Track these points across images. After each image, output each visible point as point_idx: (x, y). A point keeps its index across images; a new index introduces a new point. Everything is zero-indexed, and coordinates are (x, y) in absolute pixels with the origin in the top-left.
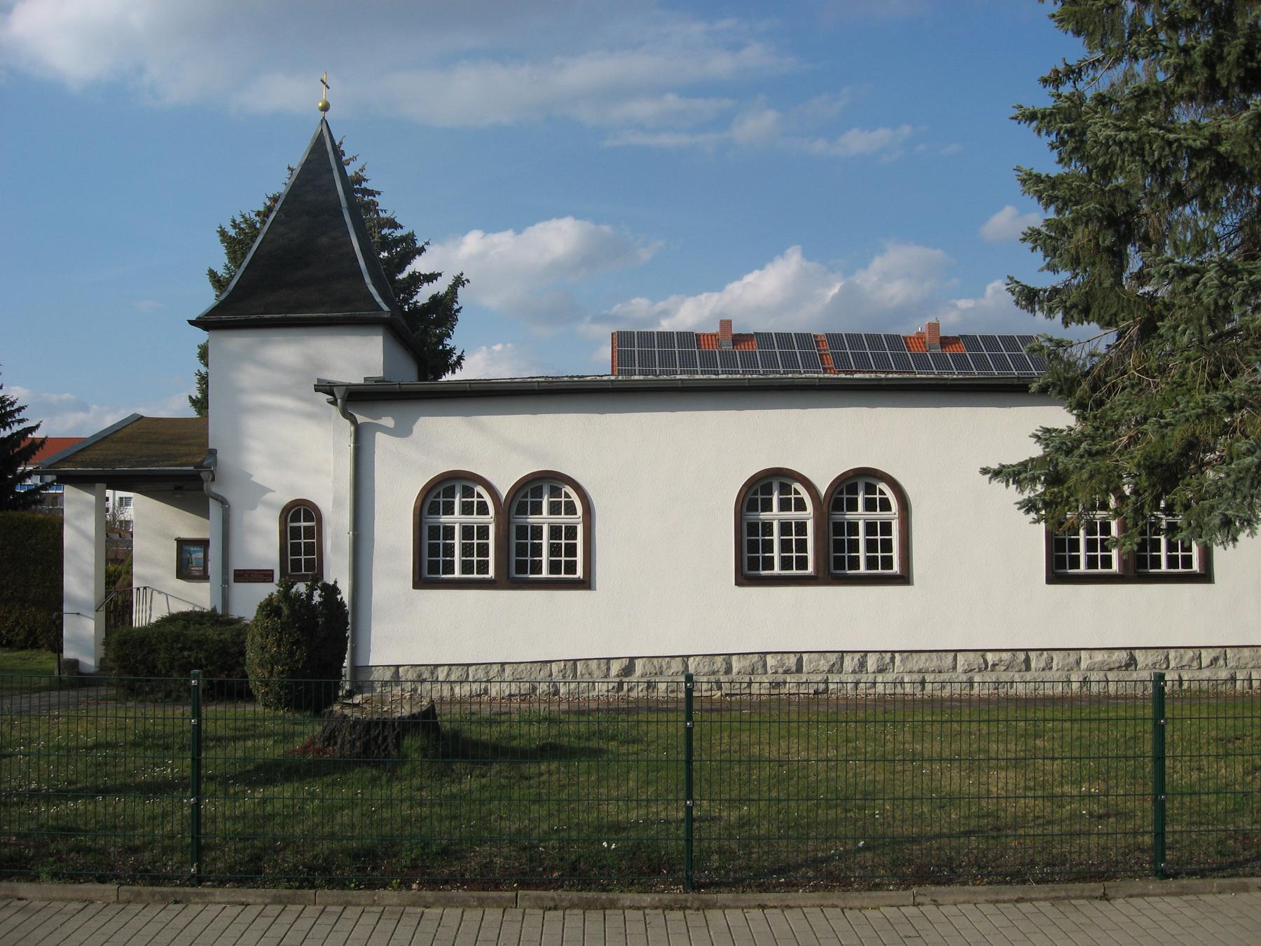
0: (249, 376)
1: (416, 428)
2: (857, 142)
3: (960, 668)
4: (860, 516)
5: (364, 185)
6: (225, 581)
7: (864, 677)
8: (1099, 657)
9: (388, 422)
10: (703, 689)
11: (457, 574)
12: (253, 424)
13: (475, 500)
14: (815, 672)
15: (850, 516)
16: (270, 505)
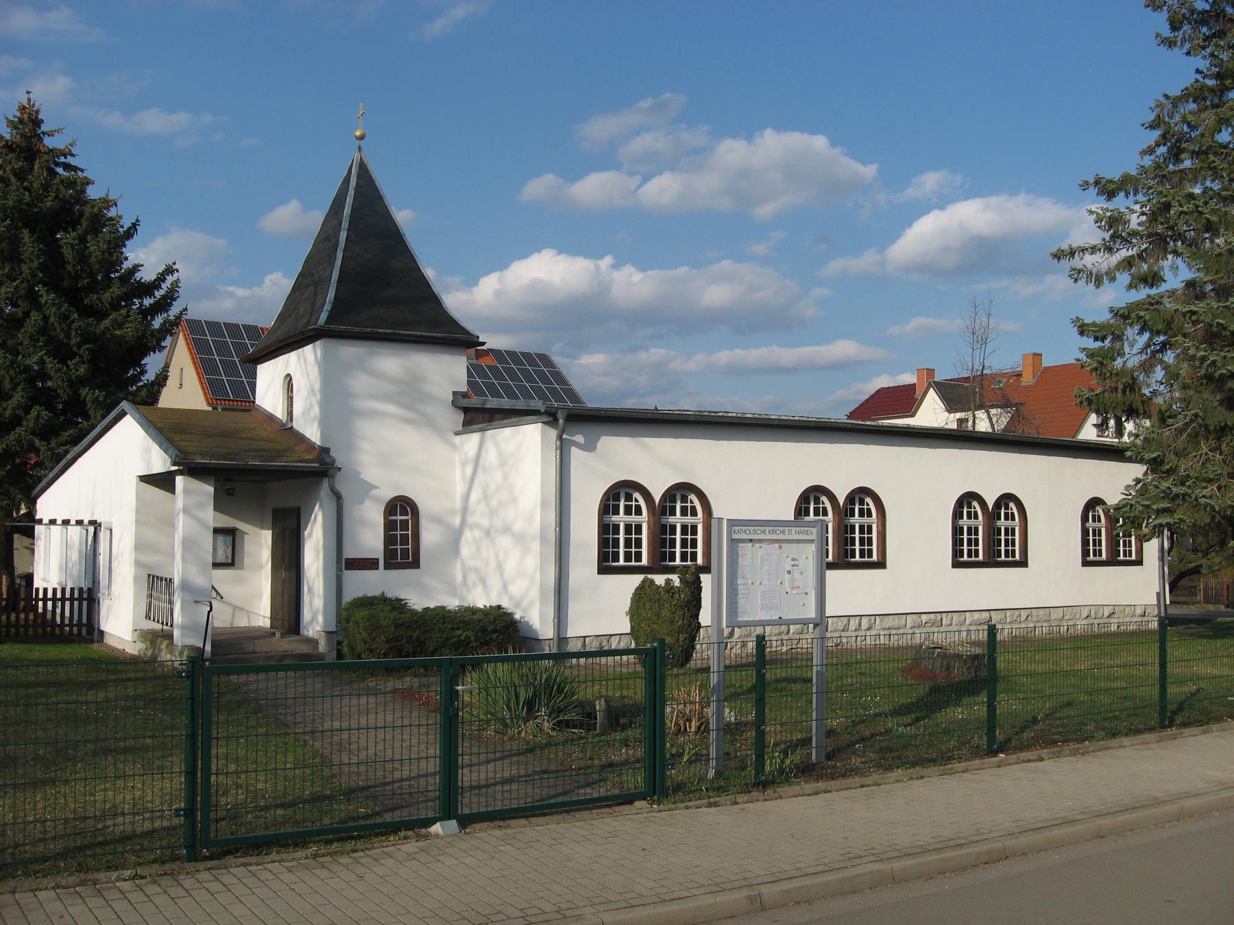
0: (360, 383)
1: (599, 445)
2: (153, 121)
3: (909, 626)
4: (677, 520)
5: (70, 160)
6: (339, 569)
7: (860, 633)
8: (976, 616)
9: (580, 439)
10: (773, 646)
11: (622, 562)
12: (365, 427)
13: (634, 503)
14: (836, 631)
15: (672, 520)
16: (376, 499)
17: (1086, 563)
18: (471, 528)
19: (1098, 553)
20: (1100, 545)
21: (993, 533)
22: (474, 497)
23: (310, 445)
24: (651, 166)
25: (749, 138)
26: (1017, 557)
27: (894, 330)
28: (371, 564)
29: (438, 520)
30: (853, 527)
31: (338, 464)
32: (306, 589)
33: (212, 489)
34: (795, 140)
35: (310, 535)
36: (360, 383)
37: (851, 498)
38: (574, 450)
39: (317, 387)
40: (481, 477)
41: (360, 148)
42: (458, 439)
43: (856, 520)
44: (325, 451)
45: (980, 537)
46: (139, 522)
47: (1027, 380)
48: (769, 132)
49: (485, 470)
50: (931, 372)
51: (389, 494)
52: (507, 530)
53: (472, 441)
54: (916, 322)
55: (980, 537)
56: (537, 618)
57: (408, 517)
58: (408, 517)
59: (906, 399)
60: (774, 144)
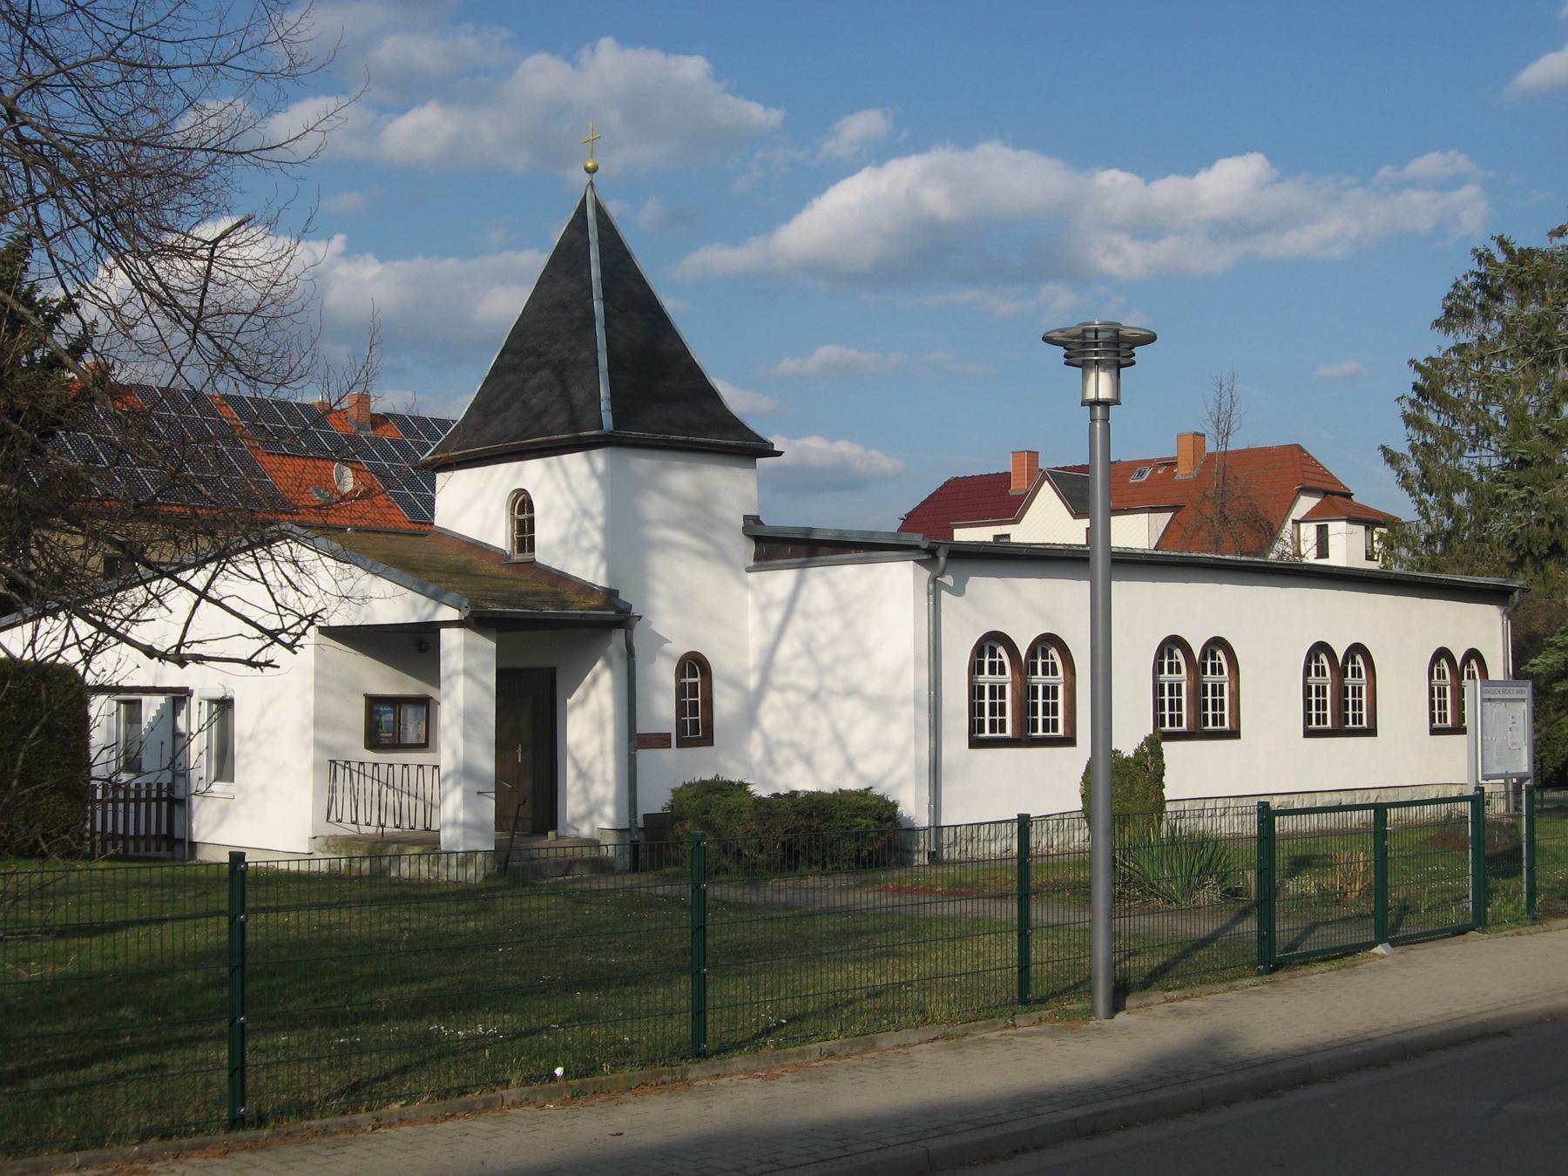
13: (997, 660)
17: (1309, 733)
18: (782, 689)
19: (1321, 719)
20: (1003, 713)
21: (1026, 695)
22: (784, 651)
23: (586, 589)
24: (410, 90)
25: (571, 57)
26: (1227, 725)
27: (788, 365)
28: (661, 741)
29: (735, 683)
30: (1035, 689)
31: (635, 611)
32: (571, 773)
33: (494, 645)
34: (649, 61)
35: (583, 702)
36: (653, 505)
37: (1032, 651)
38: (944, 594)
39: (597, 507)
40: (798, 625)
41: (592, 184)
42: (752, 576)
43: (1039, 680)
44: (611, 594)
45: (1328, 698)
46: (319, 689)
47: (1184, 472)
48: (606, 44)
49: (806, 615)
50: (1033, 456)
51: (680, 648)
52: (852, 692)
53: (781, 581)
54: (826, 353)
55: (1328, 698)
56: (912, 805)
57: (698, 680)
58: (698, 680)
59: (997, 497)
60: (611, 64)
